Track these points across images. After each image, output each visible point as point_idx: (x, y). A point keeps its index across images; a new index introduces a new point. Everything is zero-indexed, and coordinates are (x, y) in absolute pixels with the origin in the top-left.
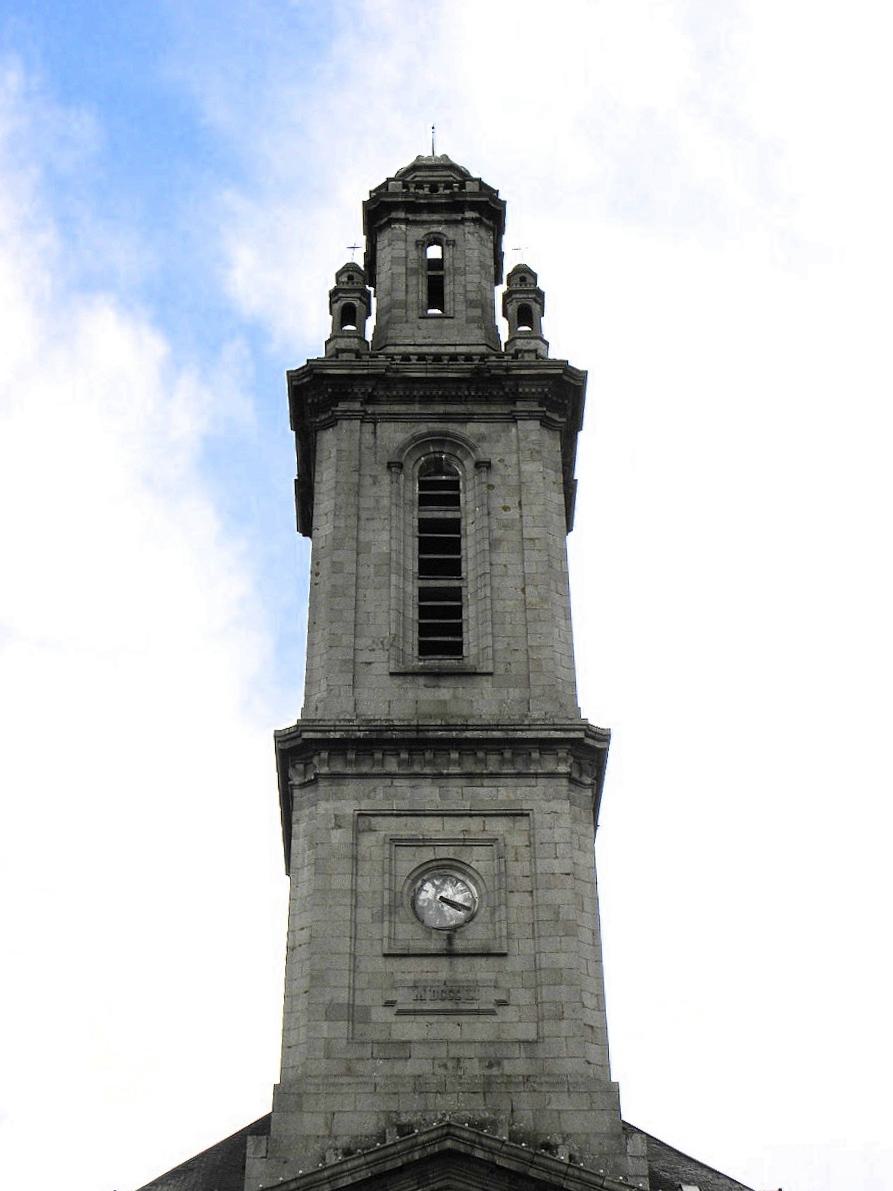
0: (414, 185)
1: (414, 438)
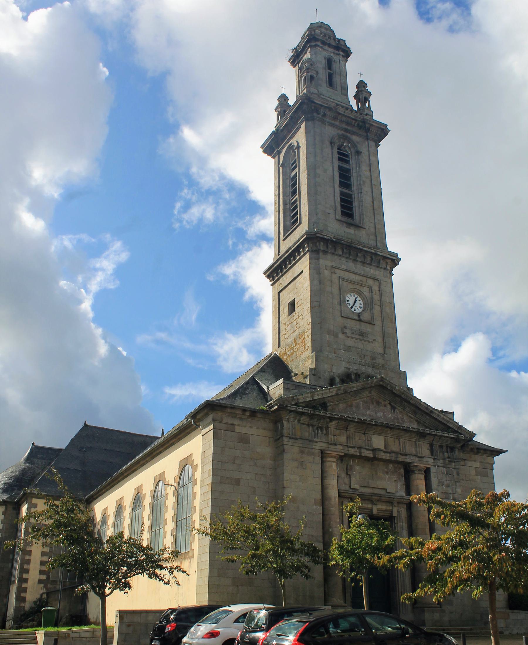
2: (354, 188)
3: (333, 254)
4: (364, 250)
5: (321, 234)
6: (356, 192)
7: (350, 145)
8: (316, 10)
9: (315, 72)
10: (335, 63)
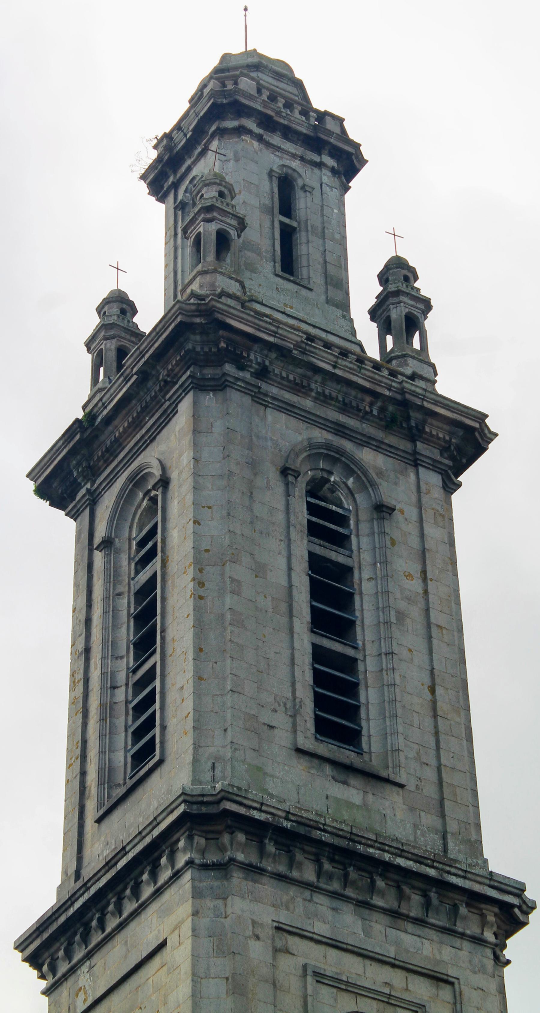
0: (300, 108)
1: (312, 445)
4: (399, 868)
6: (371, 649)
8: (246, 9)
10: (305, 191)
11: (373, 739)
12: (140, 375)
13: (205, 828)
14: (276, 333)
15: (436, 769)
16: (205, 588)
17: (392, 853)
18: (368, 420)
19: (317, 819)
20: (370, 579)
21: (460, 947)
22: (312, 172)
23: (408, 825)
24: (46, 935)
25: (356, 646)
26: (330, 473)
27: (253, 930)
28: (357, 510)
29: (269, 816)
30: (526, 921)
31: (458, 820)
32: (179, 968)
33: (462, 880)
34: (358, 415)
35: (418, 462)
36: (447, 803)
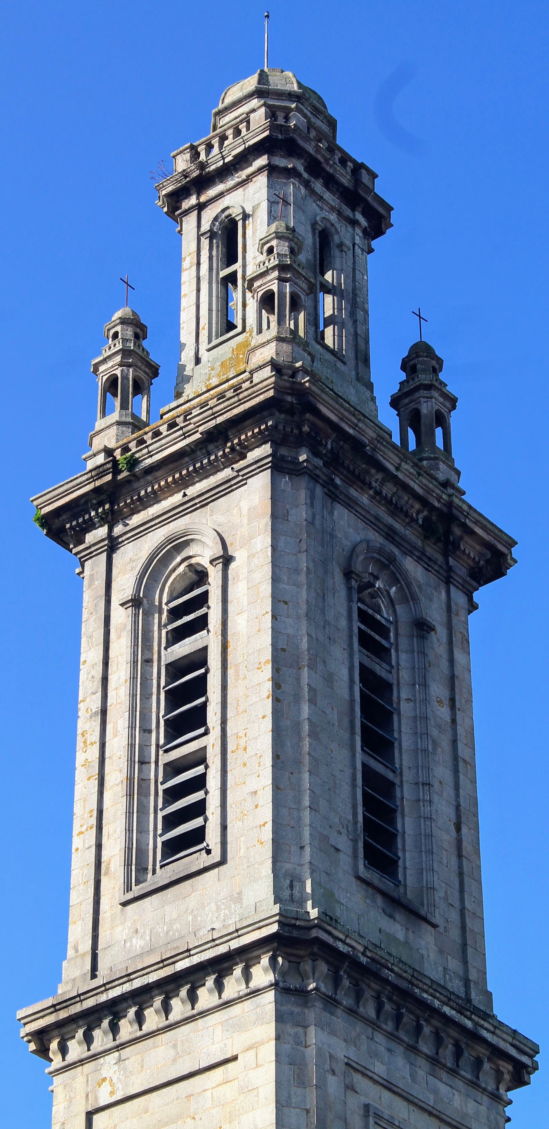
2: (401, 760)
3: (352, 1012)
5: (329, 933)
6: (408, 776)
7: (394, 588)
9: (304, 286)
10: (342, 251)
11: (408, 872)
12: (205, 436)
13: (289, 951)
14: (357, 425)
15: (459, 912)
16: (281, 690)
17: (440, 1001)
18: (411, 527)
19: (387, 957)
20: (408, 700)
21: (481, 1102)
22: (346, 229)
23: (440, 968)
24: (63, 1015)
25: (394, 769)
26: (377, 578)
27: (330, 1064)
28: (396, 622)
29: (350, 949)
30: (528, 1082)
31: (478, 969)
32: (256, 1091)
33: (491, 1035)
34: (404, 521)
35: (451, 580)
36: (470, 950)
